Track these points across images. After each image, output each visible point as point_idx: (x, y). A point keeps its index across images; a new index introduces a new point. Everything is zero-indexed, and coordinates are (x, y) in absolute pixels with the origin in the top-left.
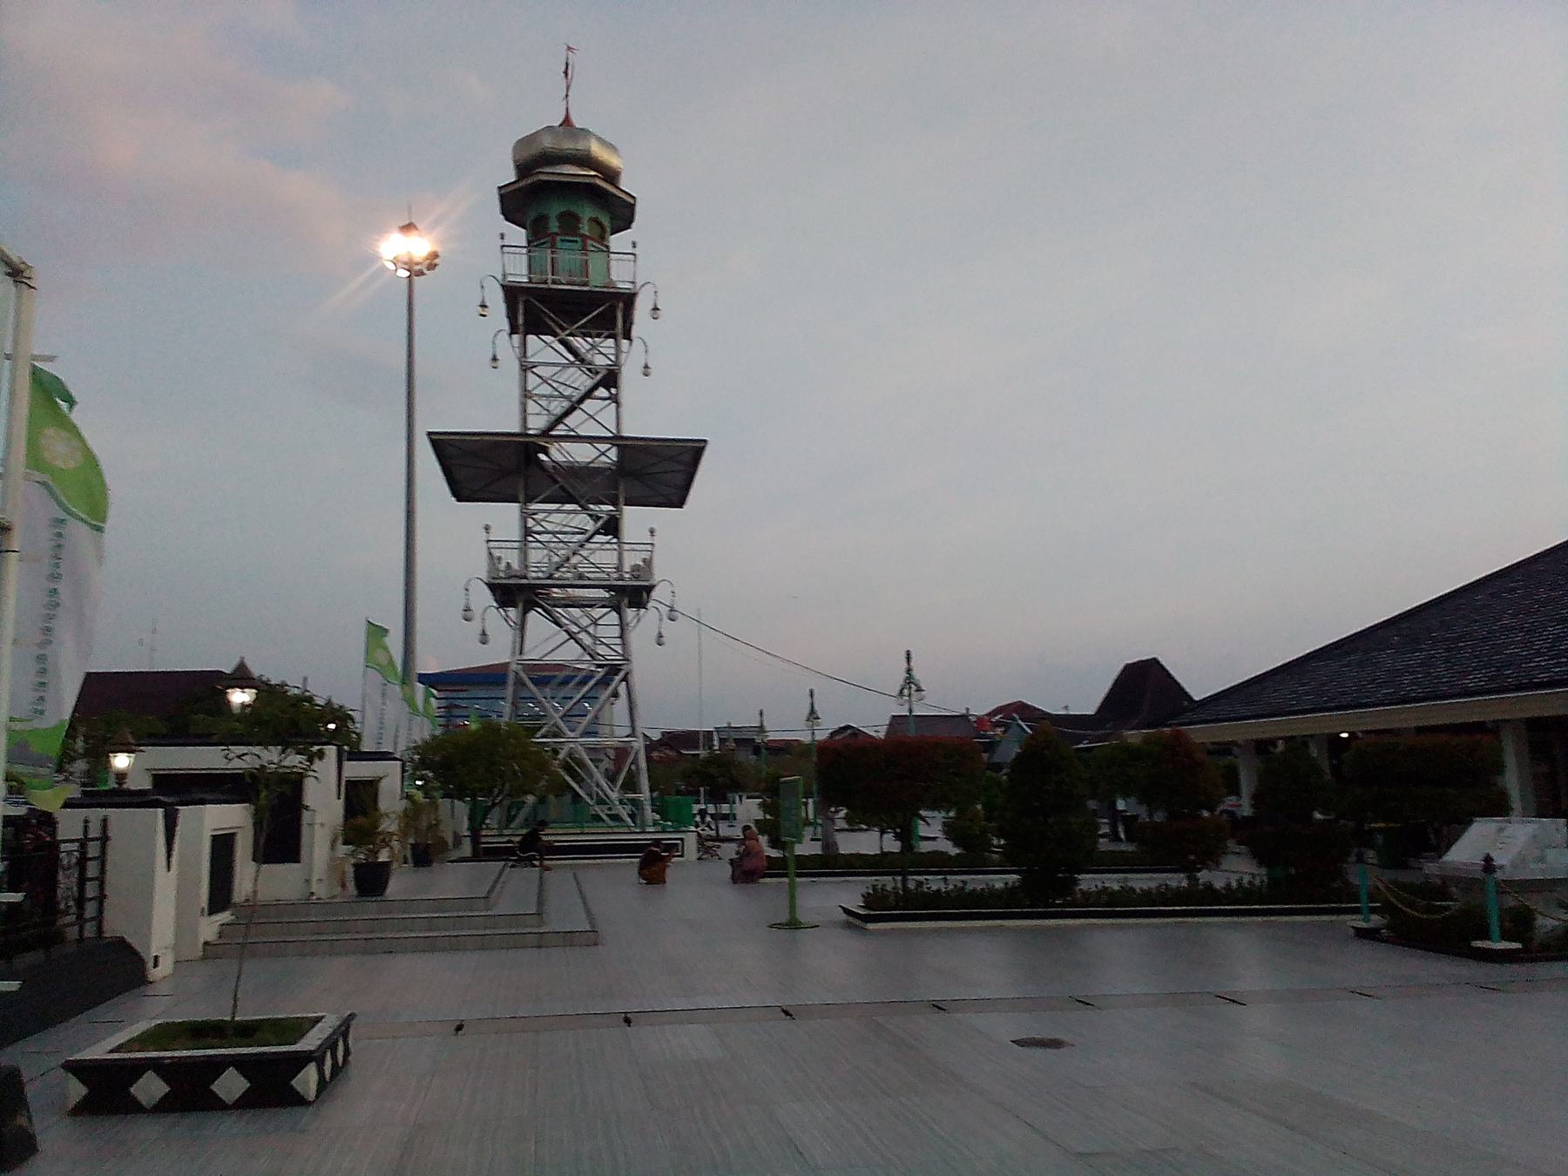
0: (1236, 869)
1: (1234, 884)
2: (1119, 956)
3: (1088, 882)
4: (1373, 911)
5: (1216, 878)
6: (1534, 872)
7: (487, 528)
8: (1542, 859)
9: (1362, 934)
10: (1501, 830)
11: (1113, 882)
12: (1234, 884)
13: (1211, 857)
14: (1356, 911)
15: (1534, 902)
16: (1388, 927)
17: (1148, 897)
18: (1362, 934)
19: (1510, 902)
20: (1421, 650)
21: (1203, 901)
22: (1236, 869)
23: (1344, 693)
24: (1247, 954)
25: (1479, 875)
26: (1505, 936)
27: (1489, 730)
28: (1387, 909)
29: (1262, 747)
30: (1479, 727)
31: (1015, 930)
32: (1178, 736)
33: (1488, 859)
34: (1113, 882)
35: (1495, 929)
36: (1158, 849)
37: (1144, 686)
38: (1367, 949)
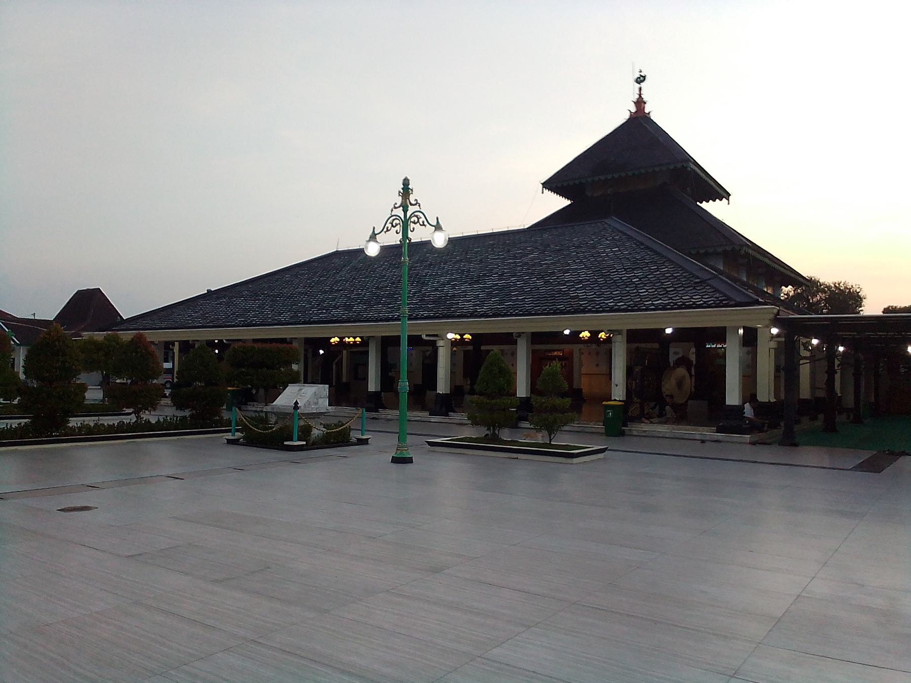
0: (166, 411)
1: (162, 420)
2: (93, 462)
3: (74, 422)
4: (237, 430)
5: (151, 417)
6: (313, 409)
7: (641, 80)
8: (317, 403)
9: (230, 442)
10: (301, 390)
11: (90, 421)
12: (162, 420)
13: (152, 405)
14: (229, 431)
15: (312, 423)
16: (243, 438)
17: (111, 429)
18: (230, 442)
19: (302, 423)
20: (259, 300)
21: (142, 430)
22: (166, 411)
23: (218, 319)
24: (163, 454)
25: (292, 411)
26: (299, 440)
27: (508, 339)
28: (245, 429)
29: (186, 346)
30: (283, 341)
31: (25, 452)
32: (140, 337)
33: (296, 403)
34: (90, 421)
35: (295, 436)
36: (116, 400)
37: (89, 306)
38: (232, 449)
